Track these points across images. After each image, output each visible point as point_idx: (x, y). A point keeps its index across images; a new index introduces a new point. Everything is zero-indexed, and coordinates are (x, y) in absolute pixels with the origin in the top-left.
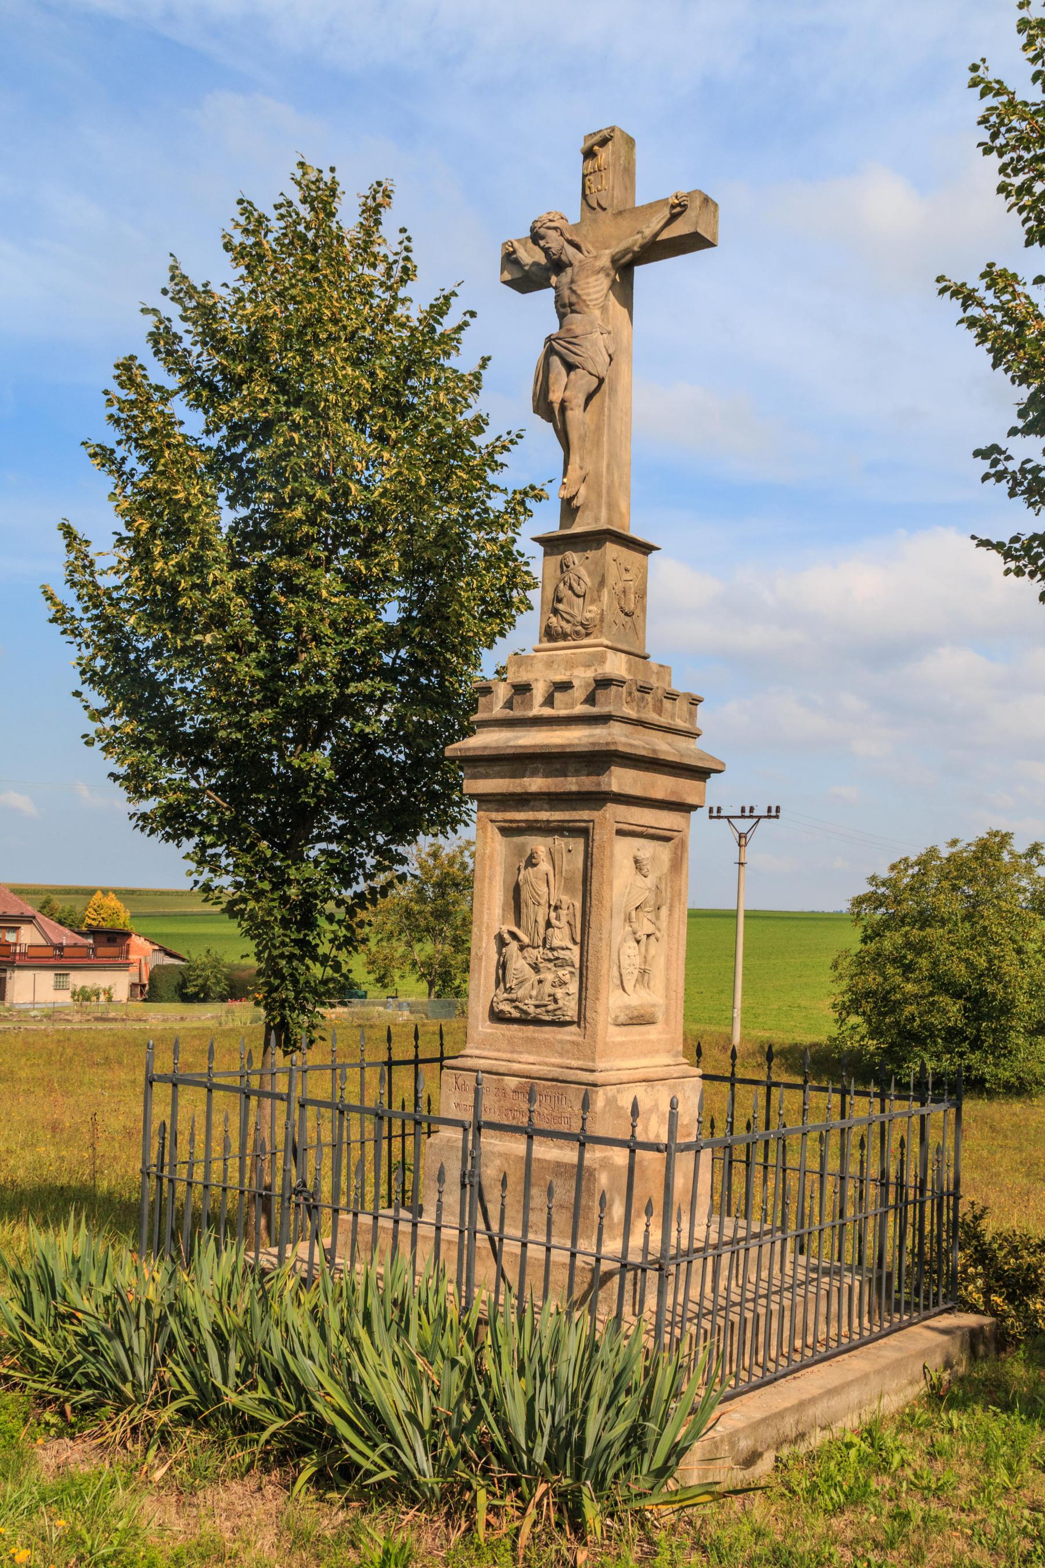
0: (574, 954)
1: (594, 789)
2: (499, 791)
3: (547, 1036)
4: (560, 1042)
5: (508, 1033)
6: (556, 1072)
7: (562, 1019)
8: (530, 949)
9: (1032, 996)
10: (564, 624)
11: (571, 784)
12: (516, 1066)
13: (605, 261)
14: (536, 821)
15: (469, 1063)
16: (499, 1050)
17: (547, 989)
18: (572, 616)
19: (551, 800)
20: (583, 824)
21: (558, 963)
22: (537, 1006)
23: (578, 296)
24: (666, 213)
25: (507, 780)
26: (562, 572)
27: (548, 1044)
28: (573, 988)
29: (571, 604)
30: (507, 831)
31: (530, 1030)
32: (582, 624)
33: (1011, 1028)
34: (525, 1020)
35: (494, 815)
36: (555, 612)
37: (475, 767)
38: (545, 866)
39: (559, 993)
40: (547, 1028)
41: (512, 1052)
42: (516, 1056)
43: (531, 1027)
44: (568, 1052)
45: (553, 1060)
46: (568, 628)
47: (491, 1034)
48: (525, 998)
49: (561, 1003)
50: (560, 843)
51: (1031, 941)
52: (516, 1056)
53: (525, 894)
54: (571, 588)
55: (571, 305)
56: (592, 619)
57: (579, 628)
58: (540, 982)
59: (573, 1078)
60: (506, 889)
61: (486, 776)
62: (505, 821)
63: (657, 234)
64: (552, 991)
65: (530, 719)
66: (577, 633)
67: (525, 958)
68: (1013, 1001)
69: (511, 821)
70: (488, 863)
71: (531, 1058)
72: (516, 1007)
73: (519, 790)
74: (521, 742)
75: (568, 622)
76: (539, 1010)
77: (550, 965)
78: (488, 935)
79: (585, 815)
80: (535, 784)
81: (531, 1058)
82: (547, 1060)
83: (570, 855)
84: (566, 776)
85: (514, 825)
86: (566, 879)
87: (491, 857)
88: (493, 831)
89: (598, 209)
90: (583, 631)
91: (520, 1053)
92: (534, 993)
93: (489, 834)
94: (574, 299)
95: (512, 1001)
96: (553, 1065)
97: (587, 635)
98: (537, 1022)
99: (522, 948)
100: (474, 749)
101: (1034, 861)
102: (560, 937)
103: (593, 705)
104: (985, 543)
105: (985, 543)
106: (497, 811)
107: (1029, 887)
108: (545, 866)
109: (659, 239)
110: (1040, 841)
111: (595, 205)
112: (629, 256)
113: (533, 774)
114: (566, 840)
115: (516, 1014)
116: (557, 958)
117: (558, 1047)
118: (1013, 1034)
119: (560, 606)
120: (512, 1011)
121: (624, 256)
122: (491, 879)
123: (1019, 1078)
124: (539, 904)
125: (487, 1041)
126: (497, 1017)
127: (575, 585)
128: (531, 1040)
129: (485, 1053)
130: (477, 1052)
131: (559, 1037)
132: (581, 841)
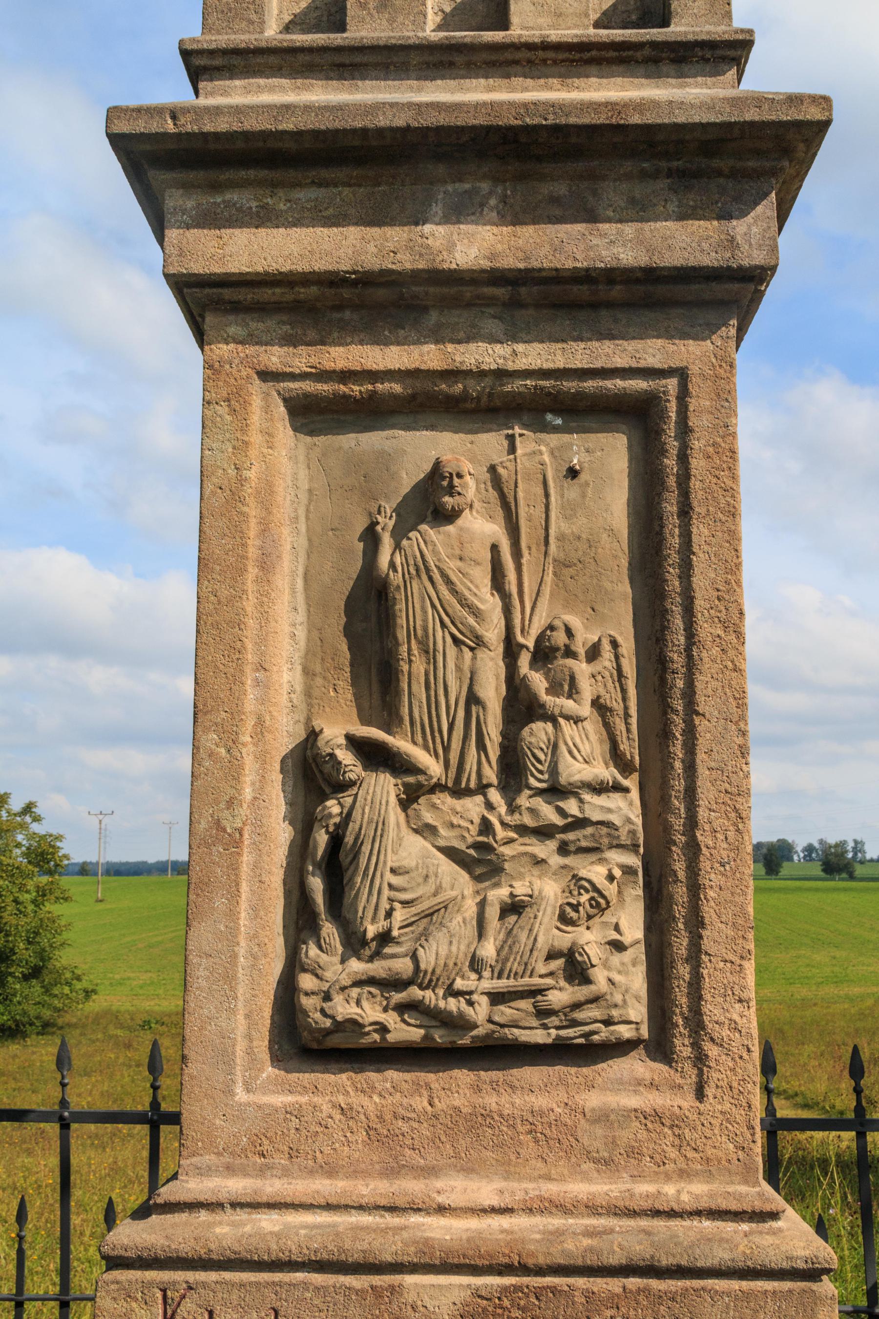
0: (625, 809)
2: (320, 265)
3: (540, 1101)
4: (602, 1117)
5: (370, 1104)
6: (627, 1240)
7: (603, 1034)
8: (444, 800)
9: (30, 943)
11: (616, 243)
12: (442, 1230)
14: (452, 374)
15: (224, 1232)
16: (330, 1171)
17: (548, 933)
20: (639, 385)
21: (574, 837)
22: (497, 998)
25: (353, 233)
27: (554, 1138)
28: (632, 922)
30: (313, 414)
31: (457, 1088)
33: (11, 974)
34: (449, 1048)
35: (275, 357)
37: (216, 187)
38: (481, 526)
39: (590, 940)
40: (531, 1074)
41: (391, 1172)
42: (412, 1187)
43: (462, 1076)
44: (634, 1153)
45: (579, 1189)
47: (295, 1112)
48: (453, 968)
49: (599, 975)
50: (537, 451)
51: (28, 892)
52: (412, 1187)
53: (413, 610)
58: (513, 908)
59: (720, 1256)
60: (315, 604)
61: (264, 218)
62: (323, 375)
64: (563, 940)
67: (427, 831)
68: (12, 950)
69: (345, 376)
70: (253, 510)
71: (486, 1192)
72: (402, 1008)
73: (406, 262)
76: (505, 1012)
77: (545, 849)
78: (262, 758)
79: (653, 351)
80: (471, 244)
81: (486, 1192)
82: (550, 1189)
83: (572, 491)
84: (592, 217)
85: (356, 389)
86: (562, 564)
87: (266, 495)
88: (266, 411)
91: (430, 1172)
92: (488, 950)
93: (256, 417)
95: (390, 984)
96: (592, 1209)
98: (498, 1052)
99: (409, 799)
101: (28, 819)
102: (583, 756)
106: (291, 341)
107: (24, 842)
108: (481, 526)
110: (33, 800)
113: (459, 212)
114: (554, 439)
115: (405, 1031)
116: (580, 823)
117: (593, 1138)
118: (10, 979)
120: (391, 1019)
122: (266, 565)
123: (15, 1021)
124: (479, 642)
125: (258, 1148)
126: (305, 1042)
128: (478, 1121)
129: (273, 1187)
130: (237, 1186)
131: (593, 1100)
132: (609, 455)
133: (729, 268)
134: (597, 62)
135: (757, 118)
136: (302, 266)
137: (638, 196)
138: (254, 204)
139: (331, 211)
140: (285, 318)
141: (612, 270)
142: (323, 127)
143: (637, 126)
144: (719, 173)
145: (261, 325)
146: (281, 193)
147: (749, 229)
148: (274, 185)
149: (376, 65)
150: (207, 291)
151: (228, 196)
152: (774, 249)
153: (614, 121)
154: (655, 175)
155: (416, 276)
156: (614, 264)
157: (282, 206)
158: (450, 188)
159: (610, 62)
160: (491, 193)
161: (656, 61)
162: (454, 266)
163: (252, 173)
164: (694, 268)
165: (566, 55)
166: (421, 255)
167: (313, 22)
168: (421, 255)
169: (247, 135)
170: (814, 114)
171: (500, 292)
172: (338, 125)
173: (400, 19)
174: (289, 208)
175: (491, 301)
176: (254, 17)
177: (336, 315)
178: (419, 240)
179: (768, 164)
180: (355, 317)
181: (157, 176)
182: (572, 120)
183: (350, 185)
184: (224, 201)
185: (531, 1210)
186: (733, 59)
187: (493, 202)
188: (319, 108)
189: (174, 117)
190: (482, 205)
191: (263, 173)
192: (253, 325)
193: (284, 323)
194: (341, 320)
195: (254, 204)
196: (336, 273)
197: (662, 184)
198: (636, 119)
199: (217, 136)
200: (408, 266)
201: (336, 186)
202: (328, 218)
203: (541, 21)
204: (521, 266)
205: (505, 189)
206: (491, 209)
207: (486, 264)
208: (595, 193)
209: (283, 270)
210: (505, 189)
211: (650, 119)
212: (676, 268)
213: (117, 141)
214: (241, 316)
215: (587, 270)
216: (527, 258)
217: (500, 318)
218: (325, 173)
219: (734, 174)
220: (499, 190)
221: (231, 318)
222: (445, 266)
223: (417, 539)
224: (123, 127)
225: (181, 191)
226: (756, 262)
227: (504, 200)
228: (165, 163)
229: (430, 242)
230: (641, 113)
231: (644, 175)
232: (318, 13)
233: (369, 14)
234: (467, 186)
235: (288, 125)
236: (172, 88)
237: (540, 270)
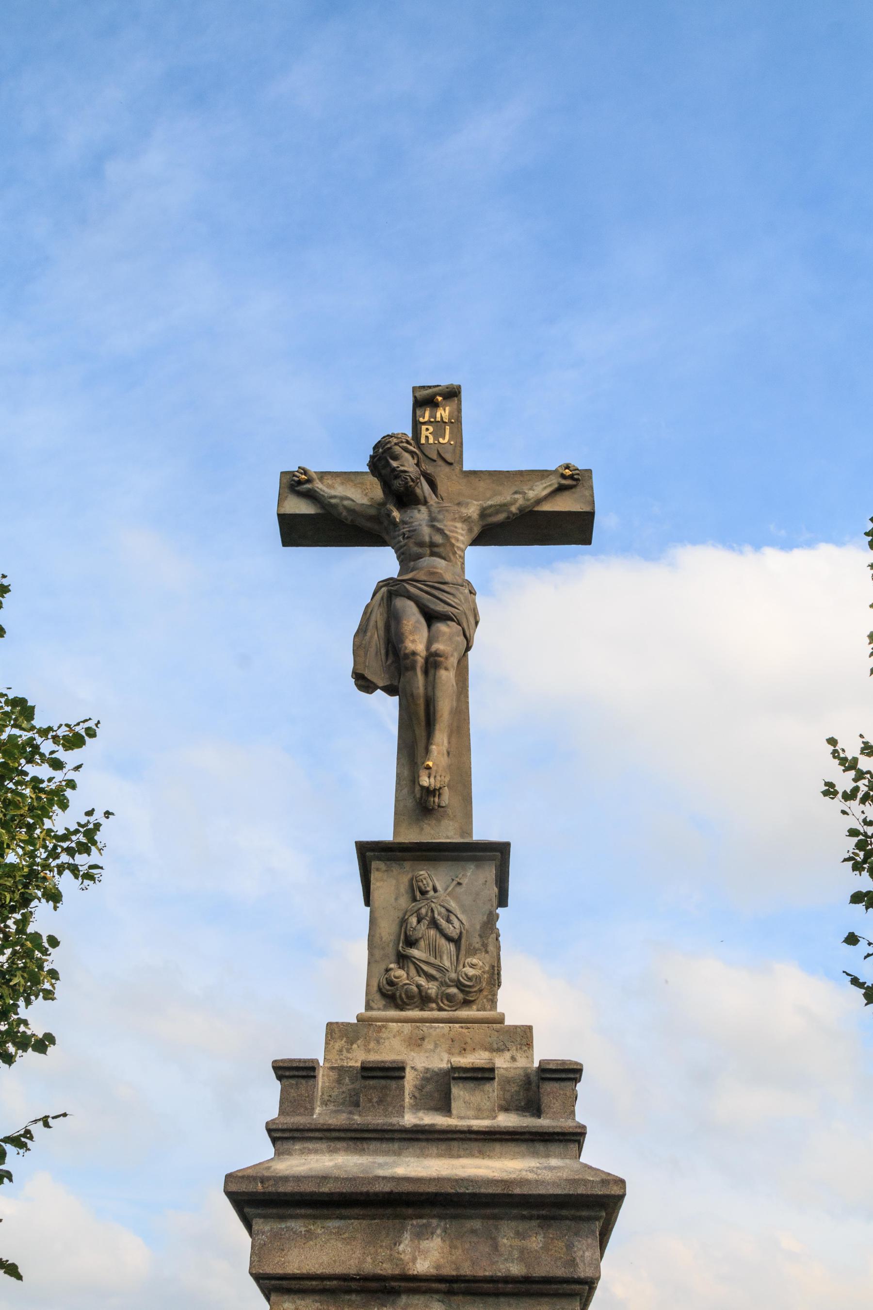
1: (560, 1272)
2: (339, 1270)
10: (422, 981)
13: (472, 510)
18: (439, 969)
19: (450, 1293)
23: (446, 537)
24: (555, 481)
26: (414, 900)
29: (435, 950)
32: (459, 985)
36: (402, 959)
37: (282, 1218)
46: (432, 988)
54: (434, 924)
55: (432, 545)
56: (478, 979)
57: (453, 990)
63: (539, 502)
65: (404, 1130)
66: (450, 998)
74: (401, 1171)
75: (430, 977)
89: (440, 462)
90: (460, 996)
94: (438, 539)
97: (467, 1003)
100: (298, 1179)
103: (538, 1112)
104: (855, 981)
105: (855, 981)
109: (536, 509)
111: (435, 457)
112: (501, 517)
119: (415, 952)
121: (497, 512)
127: (443, 922)
133: (573, 1278)
134: (500, 1140)
135: (584, 1192)
136: (328, 1271)
137: (521, 1230)
138: (303, 1229)
139: (346, 1235)
140: (317, 1298)
141: (506, 1277)
142: (344, 1191)
143: (519, 1195)
144: (567, 1218)
145: (303, 1303)
146: (319, 1222)
147: (584, 1249)
148: (315, 1217)
149: (375, 1139)
150: (273, 1282)
151: (289, 1224)
152: (598, 1268)
153: (505, 1192)
154: (531, 1218)
155: (394, 1278)
156: (508, 1274)
157: (319, 1231)
158: (415, 1222)
159: (507, 1140)
160: (438, 1226)
161: (532, 1141)
162: (415, 1273)
163: (303, 1211)
164: (552, 1277)
165: (482, 1136)
166: (397, 1265)
167: (341, 1101)
168: (397, 1265)
169: (301, 1194)
170: (615, 1190)
171: (442, 1286)
172: (353, 1190)
173: (390, 1110)
174: (324, 1232)
175: (437, 1291)
176: (308, 1106)
177: (347, 1297)
178: (396, 1255)
179: (593, 1214)
180: (359, 1298)
181: (247, 1210)
182: (483, 1191)
183: (358, 1219)
184: (286, 1227)
185: (45, 1122)
186: (575, 1141)
187: (439, 1231)
188: (343, 1179)
189: (262, 1182)
190: (432, 1233)
191: (309, 1211)
192: (299, 1302)
193: (317, 1302)
194: (349, 1300)
195: (303, 1229)
196: (348, 1275)
197: (534, 1223)
198: (517, 1191)
199: (285, 1194)
200: (390, 1272)
201: (350, 1219)
202: (345, 1239)
203: (468, 1113)
204: (454, 1273)
205: (446, 1224)
206: (438, 1236)
207: (433, 1271)
208: (497, 1228)
209: (318, 1272)
210: (446, 1224)
211: (525, 1191)
212: (542, 1277)
213: (230, 1194)
214: (292, 1296)
215: (492, 1277)
216: (457, 1269)
217: (442, 1302)
218: (344, 1212)
219: (574, 1218)
220: (442, 1224)
221: (286, 1297)
222: (411, 1272)
223: (462, 1027)
224: (233, 1188)
225: (262, 1220)
226: (588, 1275)
227: (445, 1230)
228: (255, 1200)
229: (402, 1256)
230: (520, 1187)
231: (523, 1218)
232: (344, 1095)
233: (373, 1105)
234: (425, 1221)
235: (325, 1189)
236: (258, 1152)
237: (465, 1276)
